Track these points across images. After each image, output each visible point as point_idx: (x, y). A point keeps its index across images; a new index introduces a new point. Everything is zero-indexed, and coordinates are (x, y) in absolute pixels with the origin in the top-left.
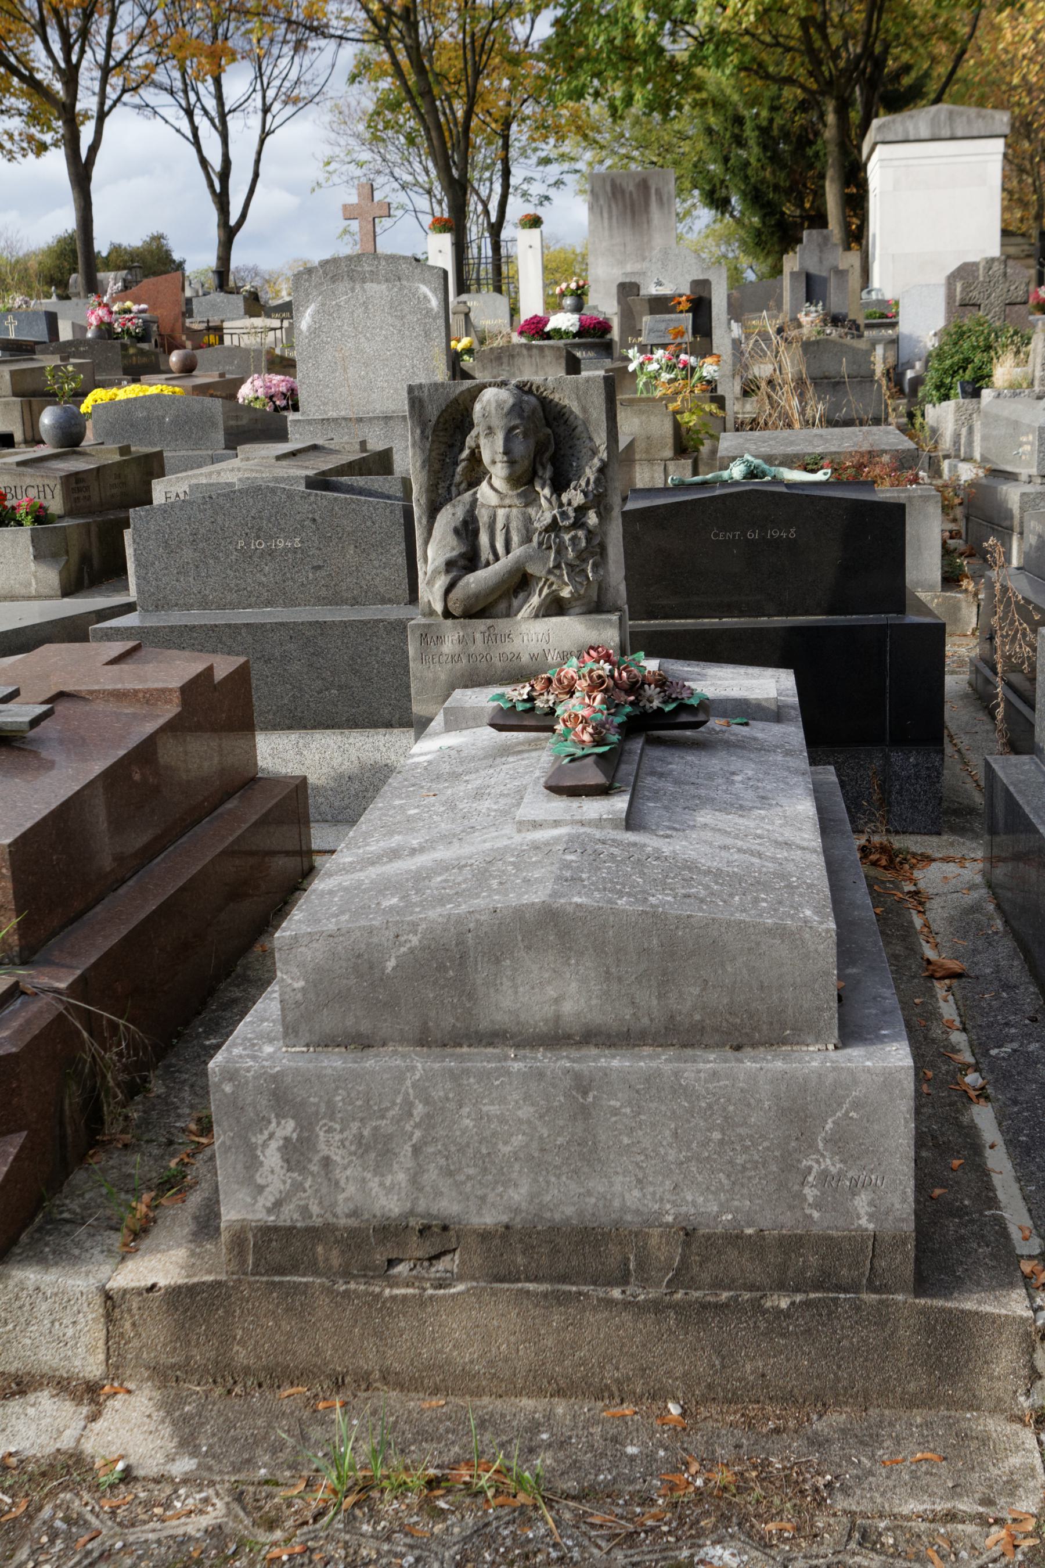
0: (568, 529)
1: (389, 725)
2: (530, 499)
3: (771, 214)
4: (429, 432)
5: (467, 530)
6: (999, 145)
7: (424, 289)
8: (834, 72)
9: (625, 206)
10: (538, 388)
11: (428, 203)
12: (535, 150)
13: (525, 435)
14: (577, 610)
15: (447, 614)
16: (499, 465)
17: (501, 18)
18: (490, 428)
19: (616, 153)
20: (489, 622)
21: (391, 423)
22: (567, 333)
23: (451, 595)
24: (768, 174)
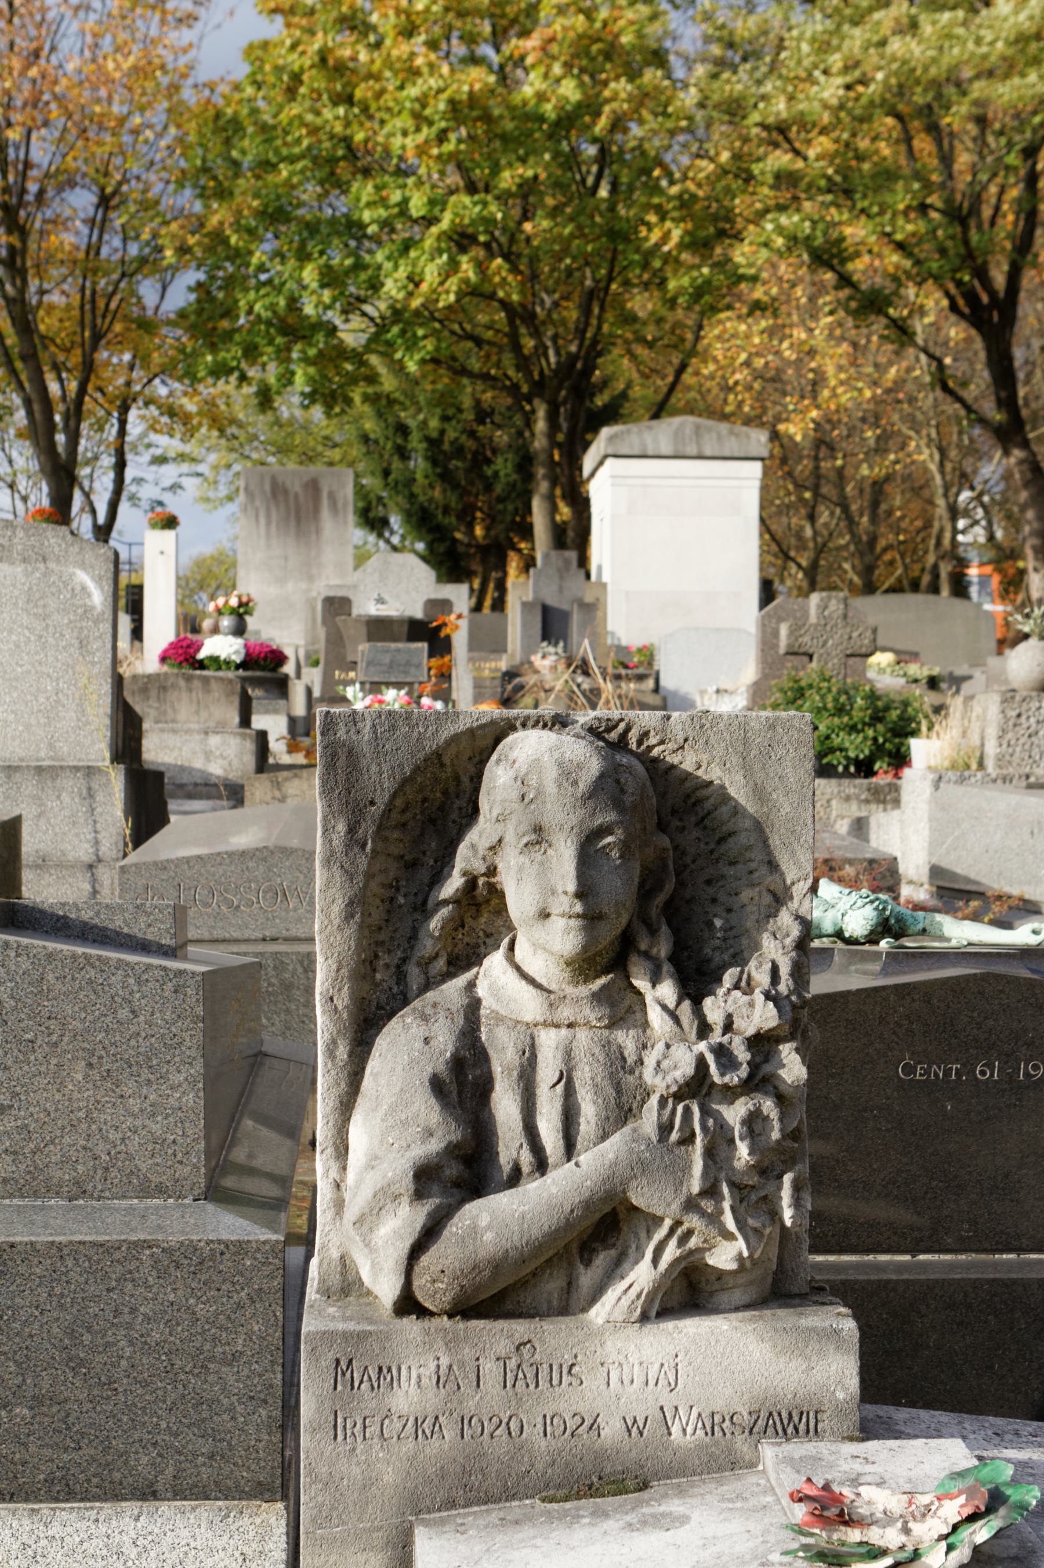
0: (730, 1094)
1: (148, 1493)
2: (622, 1008)
3: (442, 539)
4: (367, 829)
5: (461, 1083)
7: (82, 577)
8: (546, 371)
9: (288, 512)
11: (9, 500)
12: (149, 446)
13: (626, 848)
15: (408, 1305)
17: (132, 275)
18: (538, 829)
19: (248, 457)
20: (520, 1328)
21: (18, 777)
22: (228, 663)
23: (425, 1260)
24: (437, 493)
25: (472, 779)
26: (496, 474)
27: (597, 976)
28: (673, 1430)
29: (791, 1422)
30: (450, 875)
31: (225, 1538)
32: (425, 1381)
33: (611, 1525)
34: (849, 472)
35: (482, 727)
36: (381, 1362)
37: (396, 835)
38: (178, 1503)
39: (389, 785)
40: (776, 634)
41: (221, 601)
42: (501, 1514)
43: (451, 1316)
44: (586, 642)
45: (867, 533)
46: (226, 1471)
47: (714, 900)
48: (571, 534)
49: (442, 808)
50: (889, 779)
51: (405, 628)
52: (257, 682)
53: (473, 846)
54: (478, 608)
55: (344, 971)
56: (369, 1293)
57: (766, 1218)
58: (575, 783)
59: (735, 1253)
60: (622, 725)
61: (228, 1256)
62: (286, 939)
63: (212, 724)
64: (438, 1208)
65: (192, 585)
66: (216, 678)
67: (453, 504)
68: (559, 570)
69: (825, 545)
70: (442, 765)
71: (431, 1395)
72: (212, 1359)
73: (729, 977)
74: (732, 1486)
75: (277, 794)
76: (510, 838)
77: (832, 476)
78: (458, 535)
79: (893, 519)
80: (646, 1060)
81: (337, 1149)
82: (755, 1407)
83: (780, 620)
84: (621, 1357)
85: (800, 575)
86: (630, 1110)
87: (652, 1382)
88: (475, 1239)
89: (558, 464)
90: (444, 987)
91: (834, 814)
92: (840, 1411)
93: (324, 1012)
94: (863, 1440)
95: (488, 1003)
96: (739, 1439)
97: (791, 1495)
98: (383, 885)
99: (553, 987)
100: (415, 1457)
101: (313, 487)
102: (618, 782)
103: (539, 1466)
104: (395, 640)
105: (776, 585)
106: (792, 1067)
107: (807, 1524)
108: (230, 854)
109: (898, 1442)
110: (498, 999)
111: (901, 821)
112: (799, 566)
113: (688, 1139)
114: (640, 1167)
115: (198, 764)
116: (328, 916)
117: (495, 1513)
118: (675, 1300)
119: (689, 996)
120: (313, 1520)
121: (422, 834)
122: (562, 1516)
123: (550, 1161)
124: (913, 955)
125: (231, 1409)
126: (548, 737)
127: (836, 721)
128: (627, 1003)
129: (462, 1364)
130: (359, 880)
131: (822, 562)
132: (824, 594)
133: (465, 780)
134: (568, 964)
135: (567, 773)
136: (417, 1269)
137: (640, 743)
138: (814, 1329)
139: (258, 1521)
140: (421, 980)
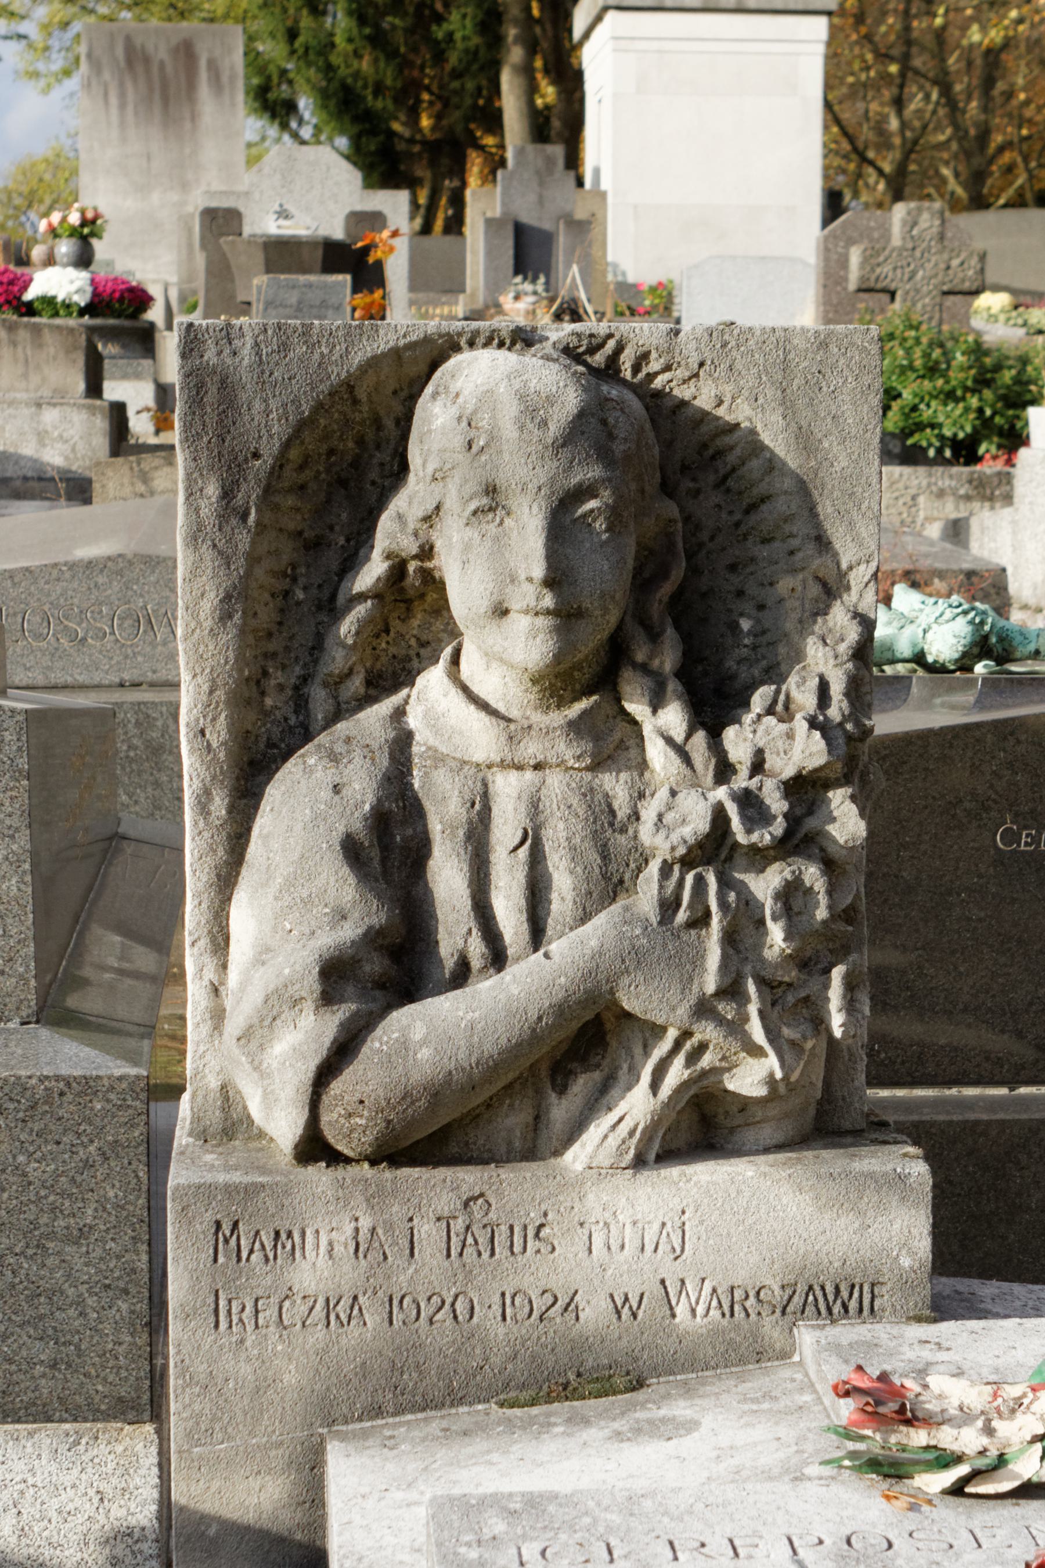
0: (760, 858)
2: (610, 742)
3: (373, 132)
4: (250, 493)
6: (819, 27)
9: (151, 90)
10: (643, 358)
13: (615, 516)
14: (768, 1133)
15: (314, 1148)
16: (520, 623)
18: (491, 490)
19: (92, 11)
22: (67, 306)
23: (336, 1087)
24: (365, 65)
25: (398, 422)
26: (450, 36)
27: (576, 699)
28: (678, 1310)
29: (839, 1298)
30: (368, 558)
31: (75, 1472)
32: (339, 1249)
33: (593, 1434)
34: (954, 32)
35: (412, 346)
36: (277, 1224)
37: (290, 501)
38: (9, 1427)
39: (279, 430)
40: (844, 263)
41: (56, 217)
42: (445, 1424)
43: (373, 1163)
44: (575, 268)
45: (977, 125)
46: (74, 1384)
47: (740, 593)
48: (556, 124)
49: (356, 464)
50: (999, 466)
51: (319, 253)
52: (111, 334)
53: (400, 517)
54: (426, 229)
55: (220, 694)
56: (261, 1134)
57: (807, 1027)
58: (544, 424)
59: (763, 1074)
60: (611, 344)
61: (69, 1097)
62: (152, 685)
63: (46, 393)
64: (355, 1016)
65: (17, 201)
66: (50, 327)
67: (389, 82)
68: (538, 173)
69: (915, 142)
70: (355, 402)
71: (347, 1267)
72: (51, 1236)
73: (759, 699)
74: (757, 1382)
75: (141, 488)
76: (452, 503)
77: (929, 40)
78: (396, 127)
79: (1014, 103)
80: (644, 814)
81: (213, 940)
82: (791, 1278)
83: (851, 242)
84: (607, 1215)
85: (881, 186)
86: (621, 882)
87: (649, 1248)
88: (405, 1058)
89: (538, 21)
90: (361, 715)
91: (922, 515)
92: (905, 1283)
93: (192, 751)
94: (935, 1321)
95: (423, 738)
96: (768, 1321)
97: (835, 1388)
98: (274, 573)
99: (514, 713)
100: (326, 1350)
101: (186, 52)
102: (604, 422)
103: (496, 1360)
104: (305, 271)
105: (847, 197)
106: (845, 821)
107: (854, 1423)
108: (72, 566)
109: (982, 1323)
110: (437, 732)
111: (1014, 522)
112: (880, 172)
113: (700, 920)
114: (634, 958)
115: (28, 449)
116: (195, 616)
117: (435, 1422)
118: (681, 1140)
119: (704, 725)
120: (189, 1435)
121: (328, 501)
122: (527, 1425)
123: (510, 952)
124: (1020, 682)
125: (79, 1302)
126: (505, 360)
127: (927, 384)
128: (617, 736)
129: (389, 1227)
130: (239, 565)
131: (913, 167)
132: (913, 205)
133: (389, 423)
134: (534, 681)
135: (532, 411)
136: (325, 1099)
137: (636, 369)
138: (871, 1175)
139: (119, 1449)
140: (329, 706)
